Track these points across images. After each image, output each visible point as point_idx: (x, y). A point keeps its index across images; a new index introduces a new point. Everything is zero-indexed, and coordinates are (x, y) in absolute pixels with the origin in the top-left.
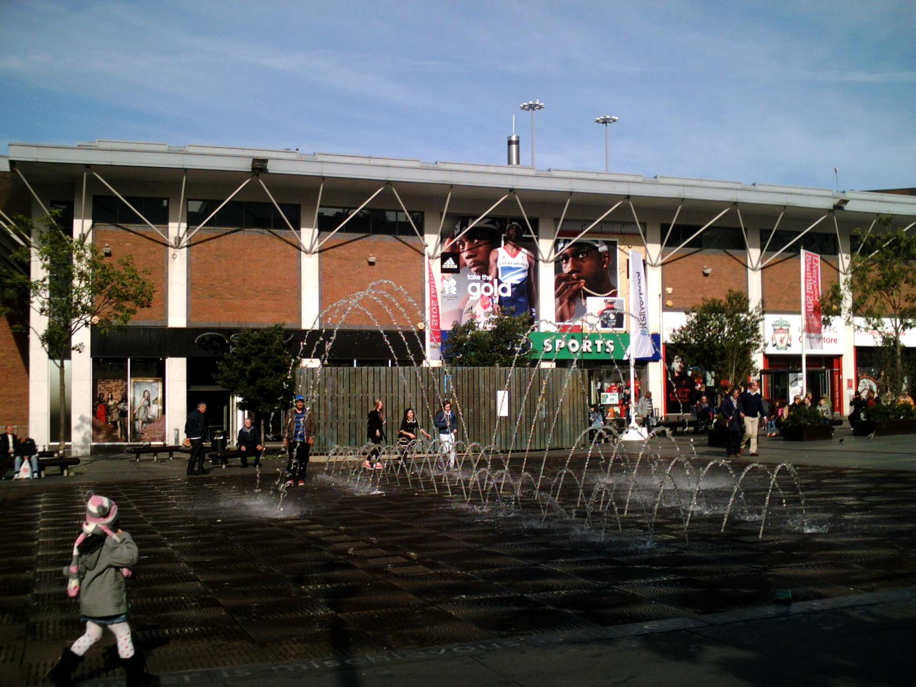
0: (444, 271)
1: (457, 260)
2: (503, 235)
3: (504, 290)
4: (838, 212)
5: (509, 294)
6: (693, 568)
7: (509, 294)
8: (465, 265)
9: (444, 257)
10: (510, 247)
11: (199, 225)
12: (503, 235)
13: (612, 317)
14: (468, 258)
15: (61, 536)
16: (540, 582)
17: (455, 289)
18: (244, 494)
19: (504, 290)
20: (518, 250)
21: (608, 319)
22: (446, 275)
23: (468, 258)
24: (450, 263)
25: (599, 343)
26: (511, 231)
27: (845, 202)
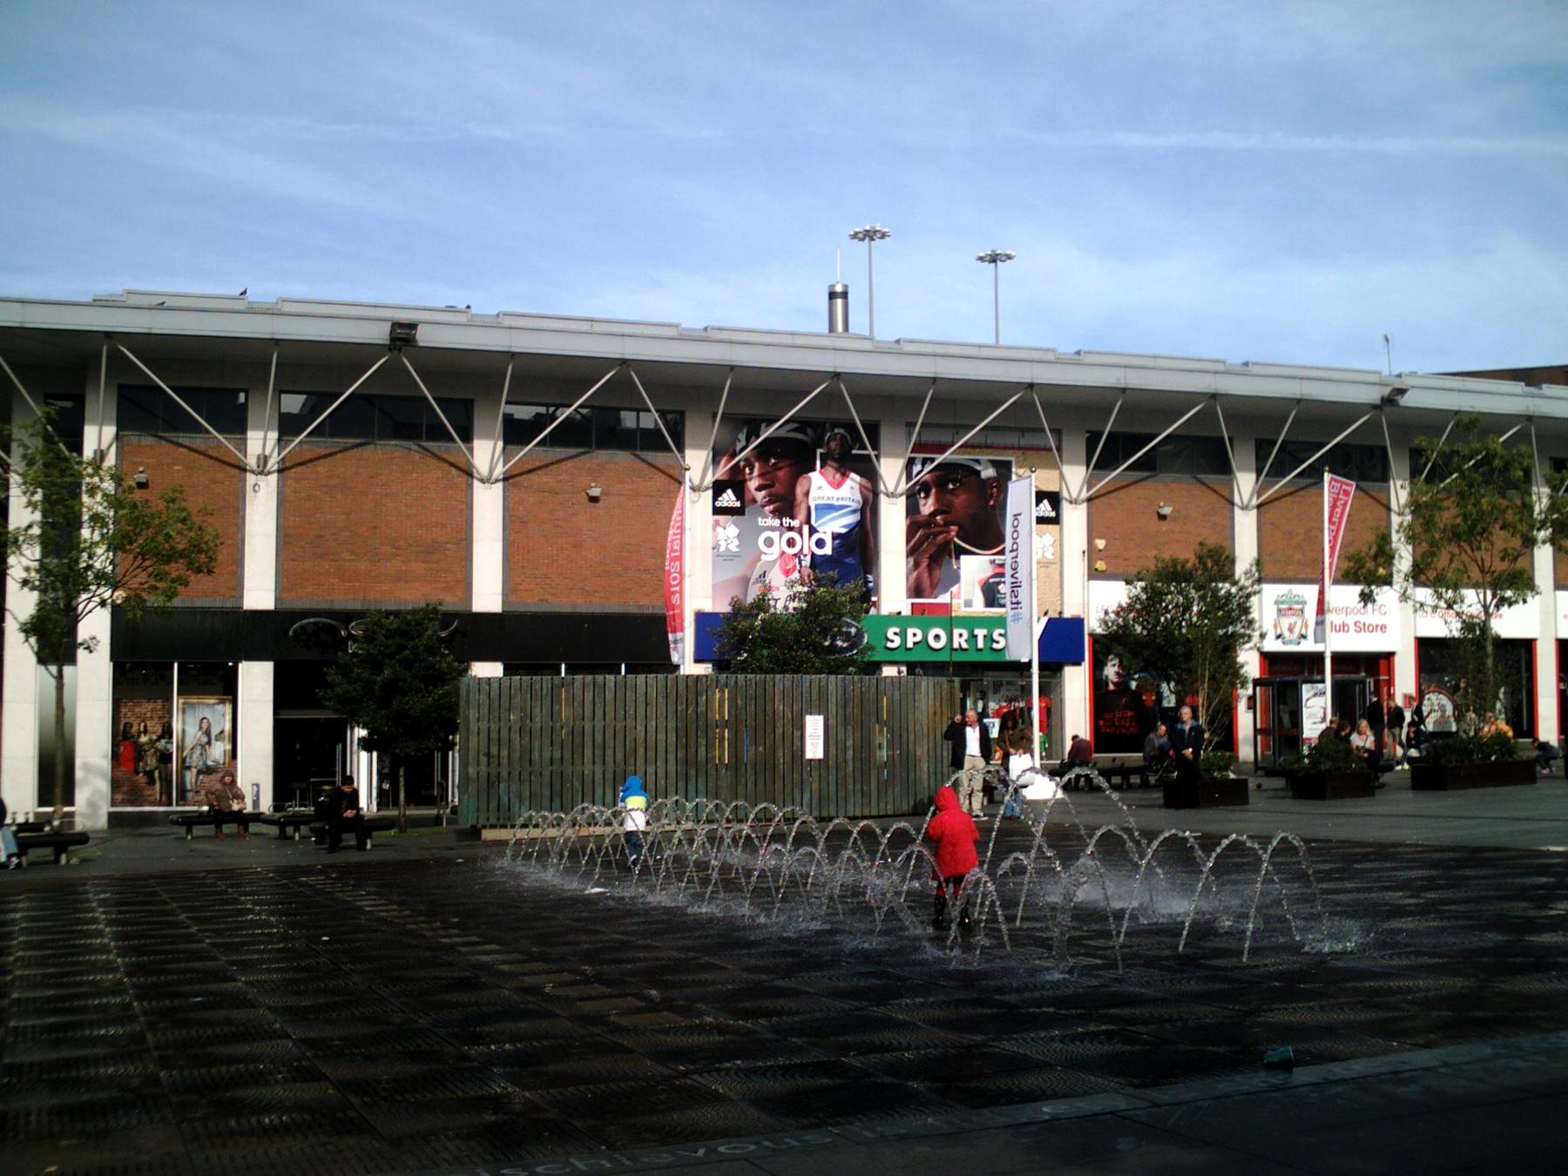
0: (717, 511)
1: (740, 495)
2: (819, 451)
4: (1387, 409)
8: (754, 501)
9: (718, 488)
10: (830, 471)
12: (819, 451)
14: (759, 489)
15: (53, 965)
17: (736, 542)
20: (845, 475)
22: (721, 518)
23: (759, 489)
24: (729, 499)
25: (980, 633)
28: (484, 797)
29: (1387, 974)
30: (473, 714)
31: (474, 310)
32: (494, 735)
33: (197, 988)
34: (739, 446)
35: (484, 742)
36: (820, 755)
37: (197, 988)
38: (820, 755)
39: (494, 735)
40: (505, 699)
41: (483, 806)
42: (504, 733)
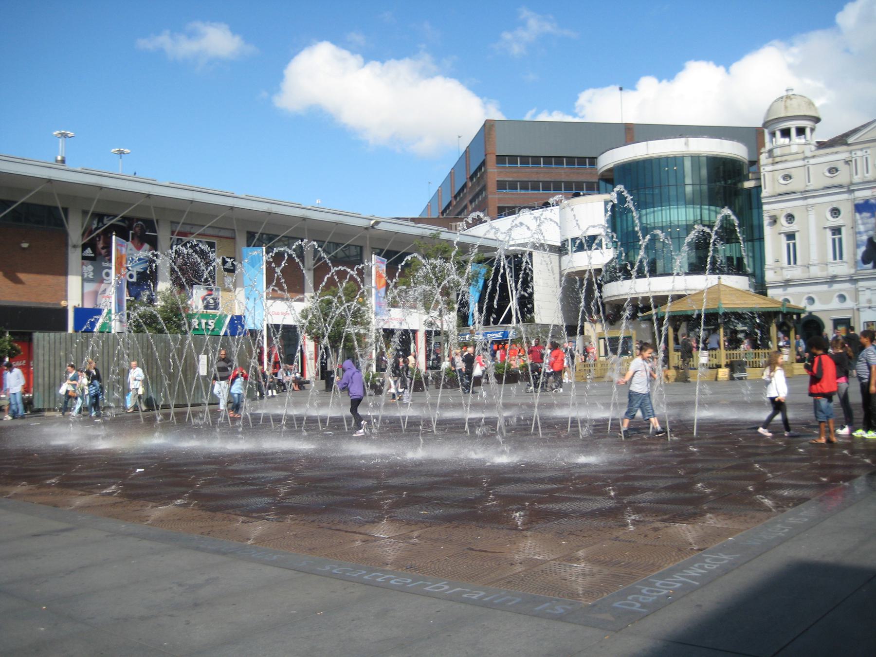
0: (84, 258)
1: (94, 250)
2: (131, 232)
3: (131, 276)
4: (371, 230)
5: (134, 280)
6: (245, 488)
7: (134, 280)
8: (100, 254)
9: (84, 247)
10: (136, 241)
11: (23, 203)
12: (131, 232)
13: (212, 301)
14: (103, 248)
15: (242, 479)
16: (219, 503)
17: (92, 274)
18: (193, 438)
19: (131, 276)
20: (142, 245)
21: (208, 302)
22: (85, 262)
23: (103, 248)
24: (89, 252)
25: (204, 321)
26: (137, 229)
27: (377, 223)
28: (47, 395)
29: (255, 471)
30: (41, 352)
31: (617, 87)
32: (52, 363)
33: (649, 484)
34: (94, 226)
35: (46, 365)
36: (205, 374)
37: (649, 484)
38: (205, 374)
39: (52, 363)
40: (57, 344)
41: (46, 399)
42: (58, 362)
